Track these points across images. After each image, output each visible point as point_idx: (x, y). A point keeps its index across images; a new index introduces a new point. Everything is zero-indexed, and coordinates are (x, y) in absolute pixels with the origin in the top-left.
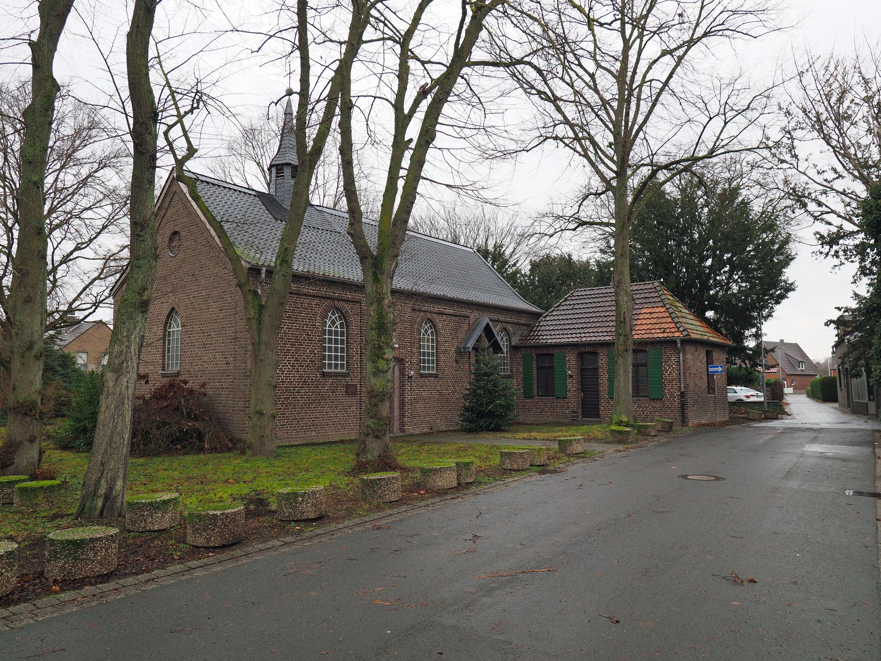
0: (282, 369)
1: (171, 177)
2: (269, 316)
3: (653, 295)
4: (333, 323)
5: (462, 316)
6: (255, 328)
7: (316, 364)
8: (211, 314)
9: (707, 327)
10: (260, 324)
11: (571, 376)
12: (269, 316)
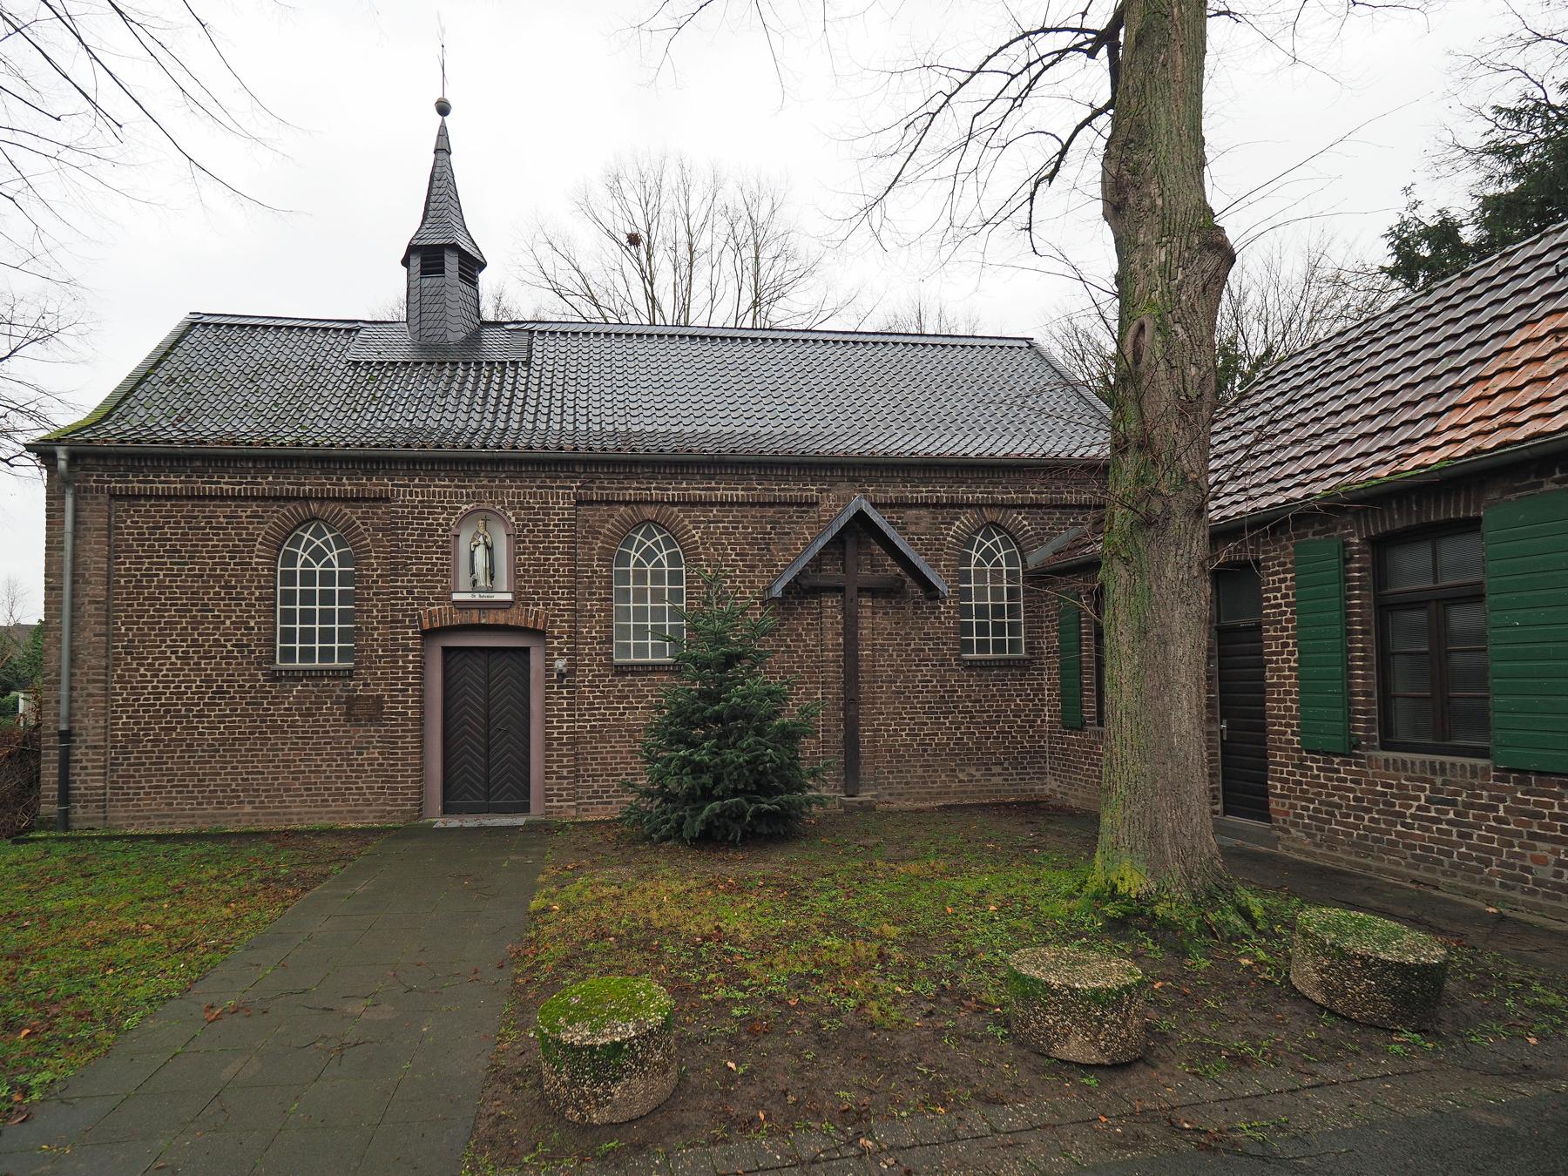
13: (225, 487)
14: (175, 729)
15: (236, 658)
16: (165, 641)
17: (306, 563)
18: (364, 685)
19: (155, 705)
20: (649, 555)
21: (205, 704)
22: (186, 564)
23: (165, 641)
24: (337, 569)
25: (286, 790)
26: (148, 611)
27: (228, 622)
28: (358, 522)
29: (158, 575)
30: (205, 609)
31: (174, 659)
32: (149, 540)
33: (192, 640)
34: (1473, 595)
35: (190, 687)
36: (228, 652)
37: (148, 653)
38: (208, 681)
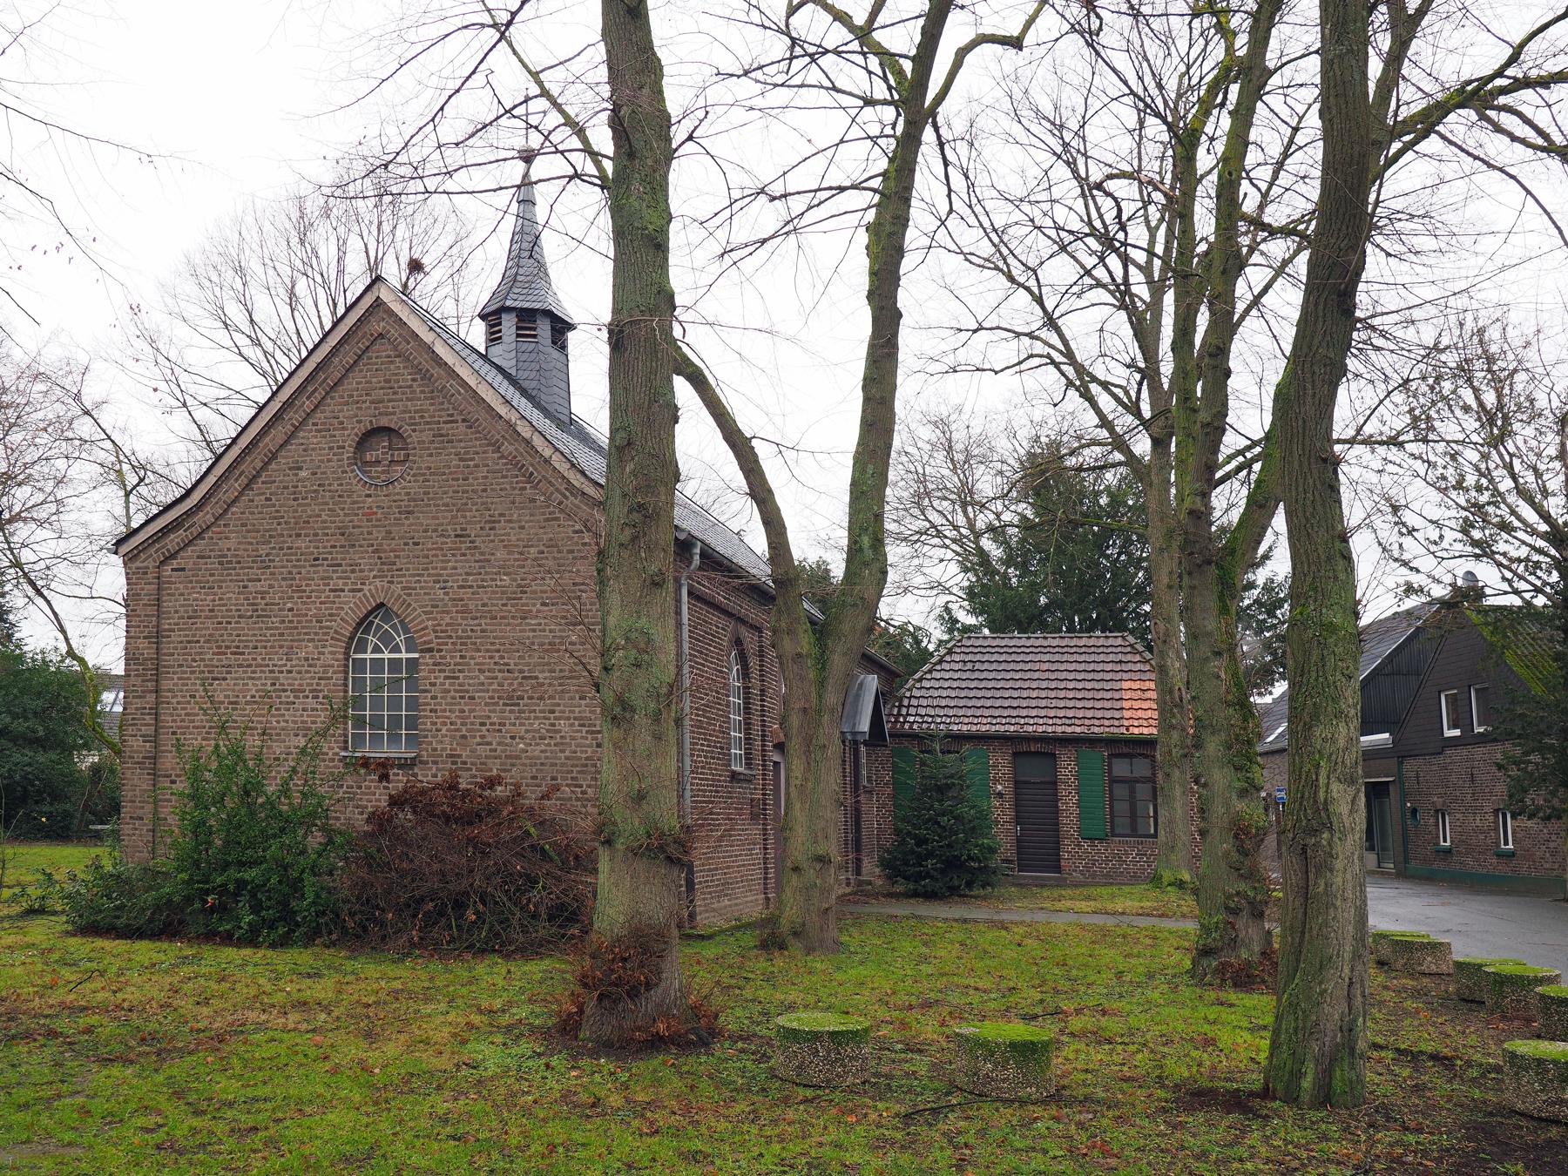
1: (368, 301)
2: (845, 654)
3: (1129, 657)
6: (811, 676)
8: (534, 631)
10: (823, 668)
11: (1000, 795)
12: (845, 654)
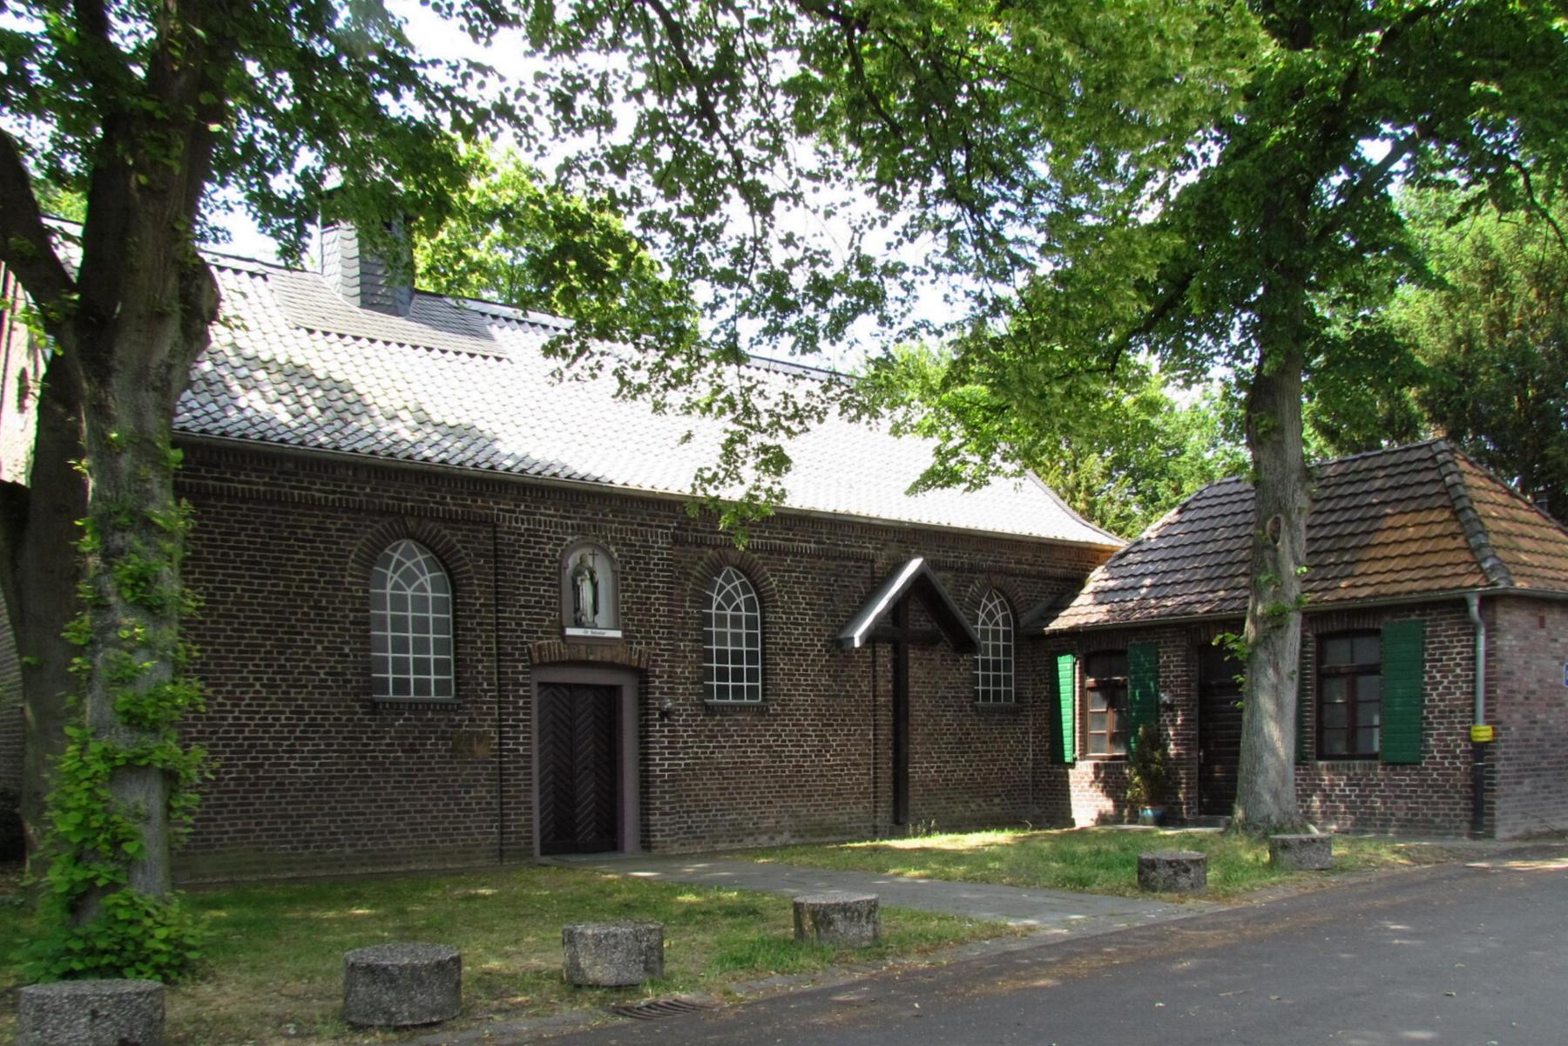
0: (233, 692)
4: (729, 599)
5: (849, 558)
7: (350, 681)
9: (539, 473)
11: (1170, 707)
13: (317, 495)
14: (262, 765)
15: (329, 687)
16: (246, 666)
17: (397, 586)
18: (471, 720)
19: (236, 739)
20: (409, 578)
21: (297, 738)
22: (268, 578)
23: (246, 666)
24: (430, 594)
25: (391, 832)
26: (224, 630)
27: (319, 648)
28: (459, 546)
29: (234, 590)
30: (292, 631)
31: (258, 686)
32: (221, 547)
33: (280, 666)
34: (1373, 670)
35: (278, 719)
36: (322, 680)
37: (227, 679)
38: (300, 712)
